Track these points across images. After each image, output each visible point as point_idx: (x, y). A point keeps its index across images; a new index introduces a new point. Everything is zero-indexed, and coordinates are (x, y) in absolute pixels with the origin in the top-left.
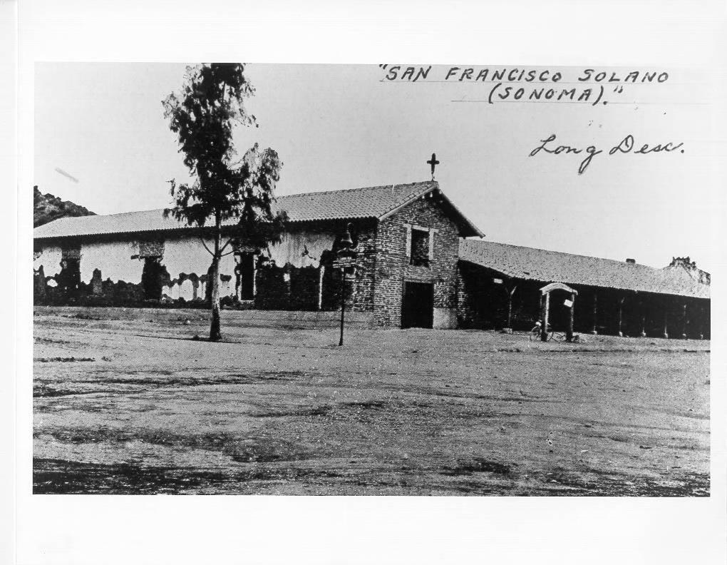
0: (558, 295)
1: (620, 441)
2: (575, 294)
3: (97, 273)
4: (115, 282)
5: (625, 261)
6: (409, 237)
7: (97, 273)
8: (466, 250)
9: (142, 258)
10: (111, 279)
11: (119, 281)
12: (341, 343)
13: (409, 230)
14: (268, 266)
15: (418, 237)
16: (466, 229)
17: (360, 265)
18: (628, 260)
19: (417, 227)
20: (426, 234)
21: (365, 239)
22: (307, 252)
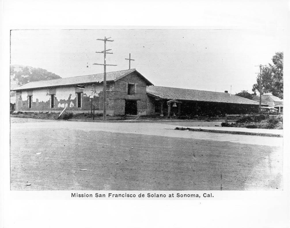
0: (172, 103)
1: (221, 133)
2: (180, 103)
3: (37, 100)
4: (93, 97)
5: (224, 92)
6: (127, 86)
7: (37, 100)
8: (149, 90)
9: (50, 95)
10: (43, 101)
11: (60, 100)
12: (30, 107)
13: (127, 84)
14: (85, 97)
15: (130, 86)
16: (149, 84)
17: (111, 96)
18: (225, 91)
19: (130, 83)
20: (133, 85)
21: (112, 87)
22: (96, 92)
